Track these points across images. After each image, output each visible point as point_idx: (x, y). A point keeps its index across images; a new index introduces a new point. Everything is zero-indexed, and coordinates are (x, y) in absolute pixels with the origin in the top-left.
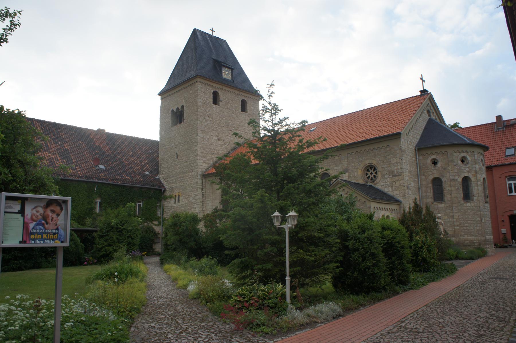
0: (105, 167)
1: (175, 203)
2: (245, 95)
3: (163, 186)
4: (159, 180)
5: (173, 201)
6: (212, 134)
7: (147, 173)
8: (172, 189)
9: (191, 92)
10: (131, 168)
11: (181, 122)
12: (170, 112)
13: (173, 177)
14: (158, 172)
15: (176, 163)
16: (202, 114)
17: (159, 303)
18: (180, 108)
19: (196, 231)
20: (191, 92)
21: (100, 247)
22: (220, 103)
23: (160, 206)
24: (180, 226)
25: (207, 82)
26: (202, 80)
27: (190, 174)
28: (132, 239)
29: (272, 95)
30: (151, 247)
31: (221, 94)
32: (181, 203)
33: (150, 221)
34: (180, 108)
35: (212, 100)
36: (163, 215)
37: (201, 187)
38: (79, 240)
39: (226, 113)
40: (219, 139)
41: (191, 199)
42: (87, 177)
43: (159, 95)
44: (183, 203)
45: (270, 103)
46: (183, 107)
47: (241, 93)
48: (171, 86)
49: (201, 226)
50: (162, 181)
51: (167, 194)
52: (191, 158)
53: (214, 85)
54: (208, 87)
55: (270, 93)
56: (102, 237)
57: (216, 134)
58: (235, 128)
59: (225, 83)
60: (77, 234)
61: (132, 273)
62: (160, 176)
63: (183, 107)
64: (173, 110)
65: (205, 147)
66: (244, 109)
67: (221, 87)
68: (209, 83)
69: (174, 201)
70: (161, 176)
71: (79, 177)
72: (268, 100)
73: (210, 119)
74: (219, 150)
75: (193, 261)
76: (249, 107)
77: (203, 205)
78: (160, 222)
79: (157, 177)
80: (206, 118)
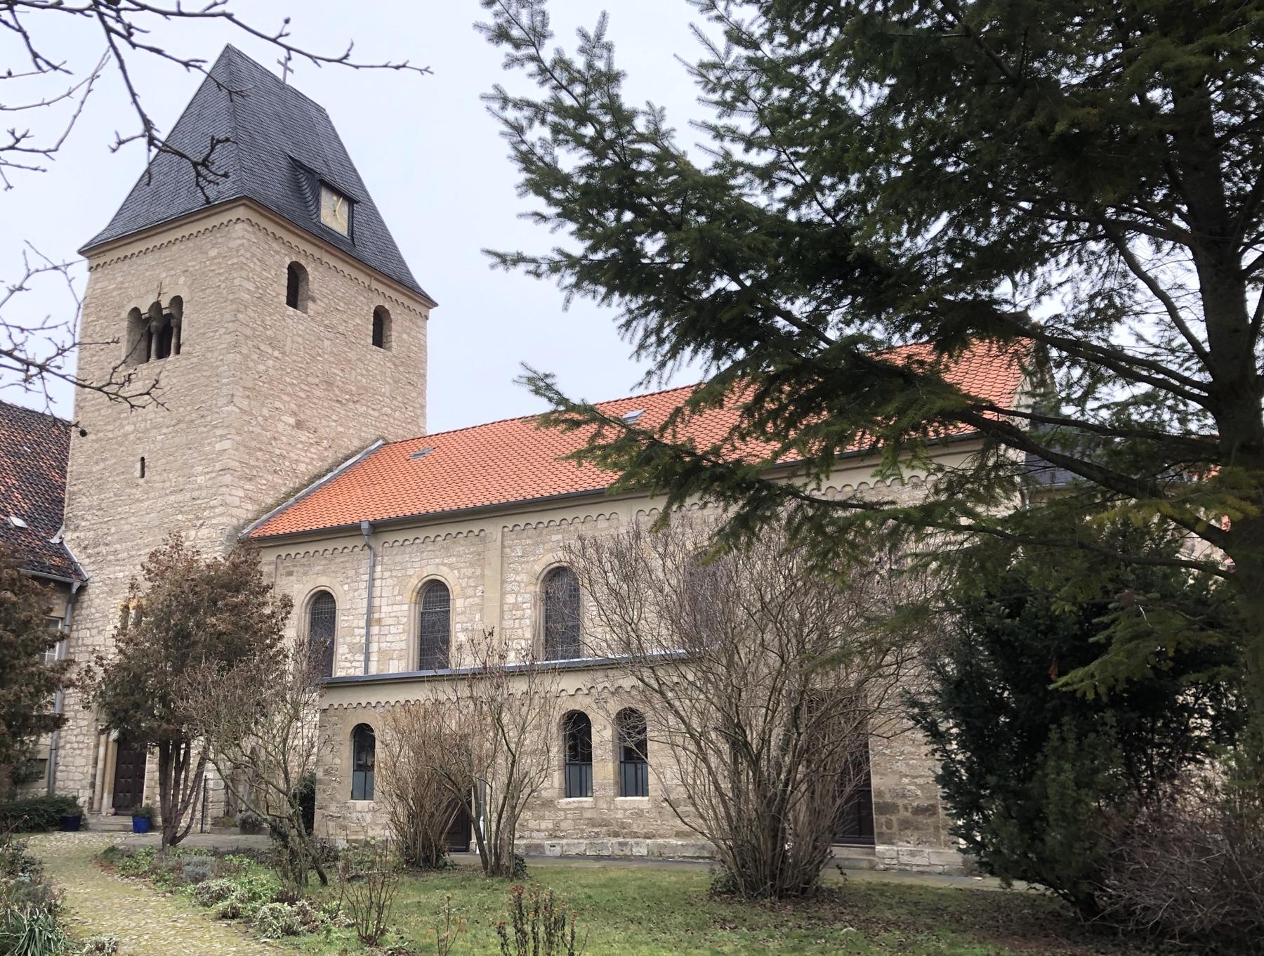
2: (389, 292)
3: (77, 573)
4: (60, 550)
6: (278, 404)
7: (19, 522)
9: (213, 253)
11: (163, 353)
12: (125, 314)
13: (120, 540)
14: (57, 522)
15: (138, 493)
16: (249, 332)
20: (213, 253)
25: (271, 228)
26: (255, 218)
31: (315, 276)
35: (285, 293)
39: (327, 343)
40: (299, 425)
43: (81, 252)
46: (177, 301)
47: (375, 285)
48: (118, 231)
50: (75, 554)
53: (295, 241)
54: (275, 245)
59: (324, 238)
62: (68, 538)
63: (177, 301)
64: (136, 311)
65: (254, 444)
66: (379, 339)
68: (280, 232)
70: (68, 536)
73: (276, 354)
76: (397, 331)
79: (55, 540)
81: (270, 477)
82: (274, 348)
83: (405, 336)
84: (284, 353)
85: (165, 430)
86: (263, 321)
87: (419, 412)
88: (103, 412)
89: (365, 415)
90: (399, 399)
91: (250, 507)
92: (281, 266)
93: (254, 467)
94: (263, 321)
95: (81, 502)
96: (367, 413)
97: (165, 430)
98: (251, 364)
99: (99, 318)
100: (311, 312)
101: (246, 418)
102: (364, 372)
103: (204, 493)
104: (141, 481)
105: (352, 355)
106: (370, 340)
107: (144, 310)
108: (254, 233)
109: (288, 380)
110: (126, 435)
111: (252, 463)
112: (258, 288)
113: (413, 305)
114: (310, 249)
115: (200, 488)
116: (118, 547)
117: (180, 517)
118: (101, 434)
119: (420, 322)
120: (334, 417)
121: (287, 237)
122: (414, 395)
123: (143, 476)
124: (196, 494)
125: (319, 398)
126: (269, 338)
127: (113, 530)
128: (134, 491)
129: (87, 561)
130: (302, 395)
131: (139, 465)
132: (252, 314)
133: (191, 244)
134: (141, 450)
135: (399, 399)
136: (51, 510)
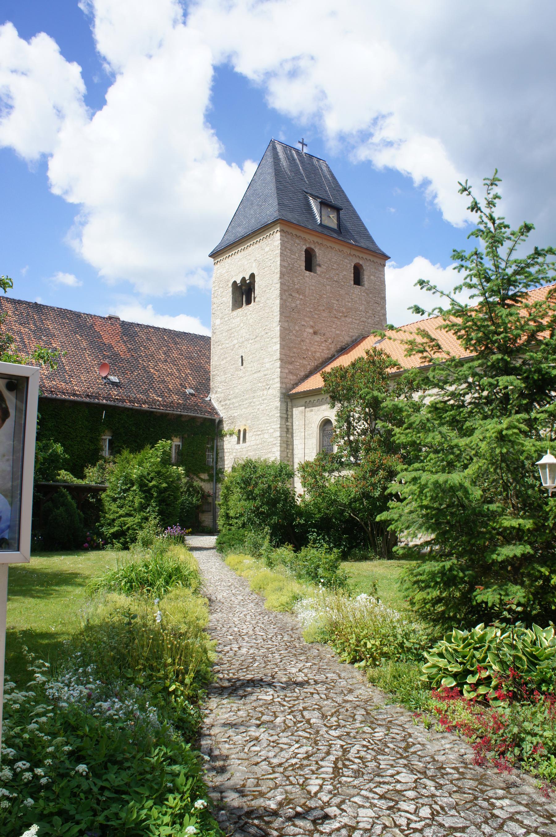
0: (119, 379)
1: (238, 442)
2: (361, 255)
4: (209, 403)
5: (235, 438)
6: (303, 323)
8: (233, 420)
9: (267, 249)
10: (163, 381)
11: (249, 302)
13: (235, 397)
14: (208, 390)
15: (240, 373)
17: (244, 651)
18: (247, 278)
19: (287, 496)
20: (267, 249)
21: (111, 517)
22: (319, 270)
23: (212, 448)
24: (257, 484)
25: (294, 232)
27: (265, 392)
28: (167, 505)
29: (496, 201)
30: (197, 517)
32: (248, 443)
33: (194, 474)
34: (247, 278)
35: (304, 264)
36: (217, 463)
37: (286, 416)
38: (75, 505)
39: (328, 287)
40: (315, 333)
41: (266, 436)
42: (88, 395)
43: (210, 256)
44: (253, 443)
45: (492, 219)
46: (252, 276)
47: (353, 252)
49: (299, 487)
51: (226, 427)
52: (268, 365)
53: (307, 237)
54: (297, 241)
55: (491, 196)
56: (114, 500)
57: (311, 323)
58: (343, 312)
60: (70, 493)
61: (176, 576)
63: (252, 276)
64: (235, 282)
65: (292, 345)
66: (358, 280)
67: (320, 241)
68: (299, 233)
69: (236, 439)
71: (75, 395)
72: (487, 211)
73: (301, 297)
74: (315, 352)
75: (286, 552)
76: (366, 277)
77: (287, 448)
78: (211, 476)
79: (208, 399)
80: (294, 294)
81: (301, 361)
82: (299, 295)
83: (372, 277)
84: (305, 296)
85: (251, 341)
86: (293, 281)
87: (382, 318)
88: (224, 334)
89: (352, 323)
90: (370, 312)
91: (291, 377)
92: (302, 251)
93: (292, 357)
94: (293, 281)
95: (218, 381)
96: (352, 322)
97: (251, 341)
98: (288, 304)
99: (220, 288)
100: (318, 272)
101: (287, 332)
102: (350, 300)
103: (269, 372)
104: (242, 367)
105: (342, 292)
106: (352, 282)
107: (238, 282)
108: (286, 236)
109: (308, 309)
110: (234, 345)
111: (291, 355)
112: (289, 264)
113: (376, 260)
114: (316, 239)
115: (267, 369)
116: (234, 400)
117: (259, 384)
118: (224, 346)
119: (380, 268)
120: (334, 326)
121: (303, 235)
122: (379, 309)
123: (242, 365)
124: (266, 372)
125: (325, 317)
126: (297, 289)
127: (231, 392)
128: (239, 373)
129: (221, 408)
130: (316, 316)
131: (240, 360)
132: (287, 278)
133: (257, 246)
134: (241, 352)
135: (370, 312)
136: (204, 386)
